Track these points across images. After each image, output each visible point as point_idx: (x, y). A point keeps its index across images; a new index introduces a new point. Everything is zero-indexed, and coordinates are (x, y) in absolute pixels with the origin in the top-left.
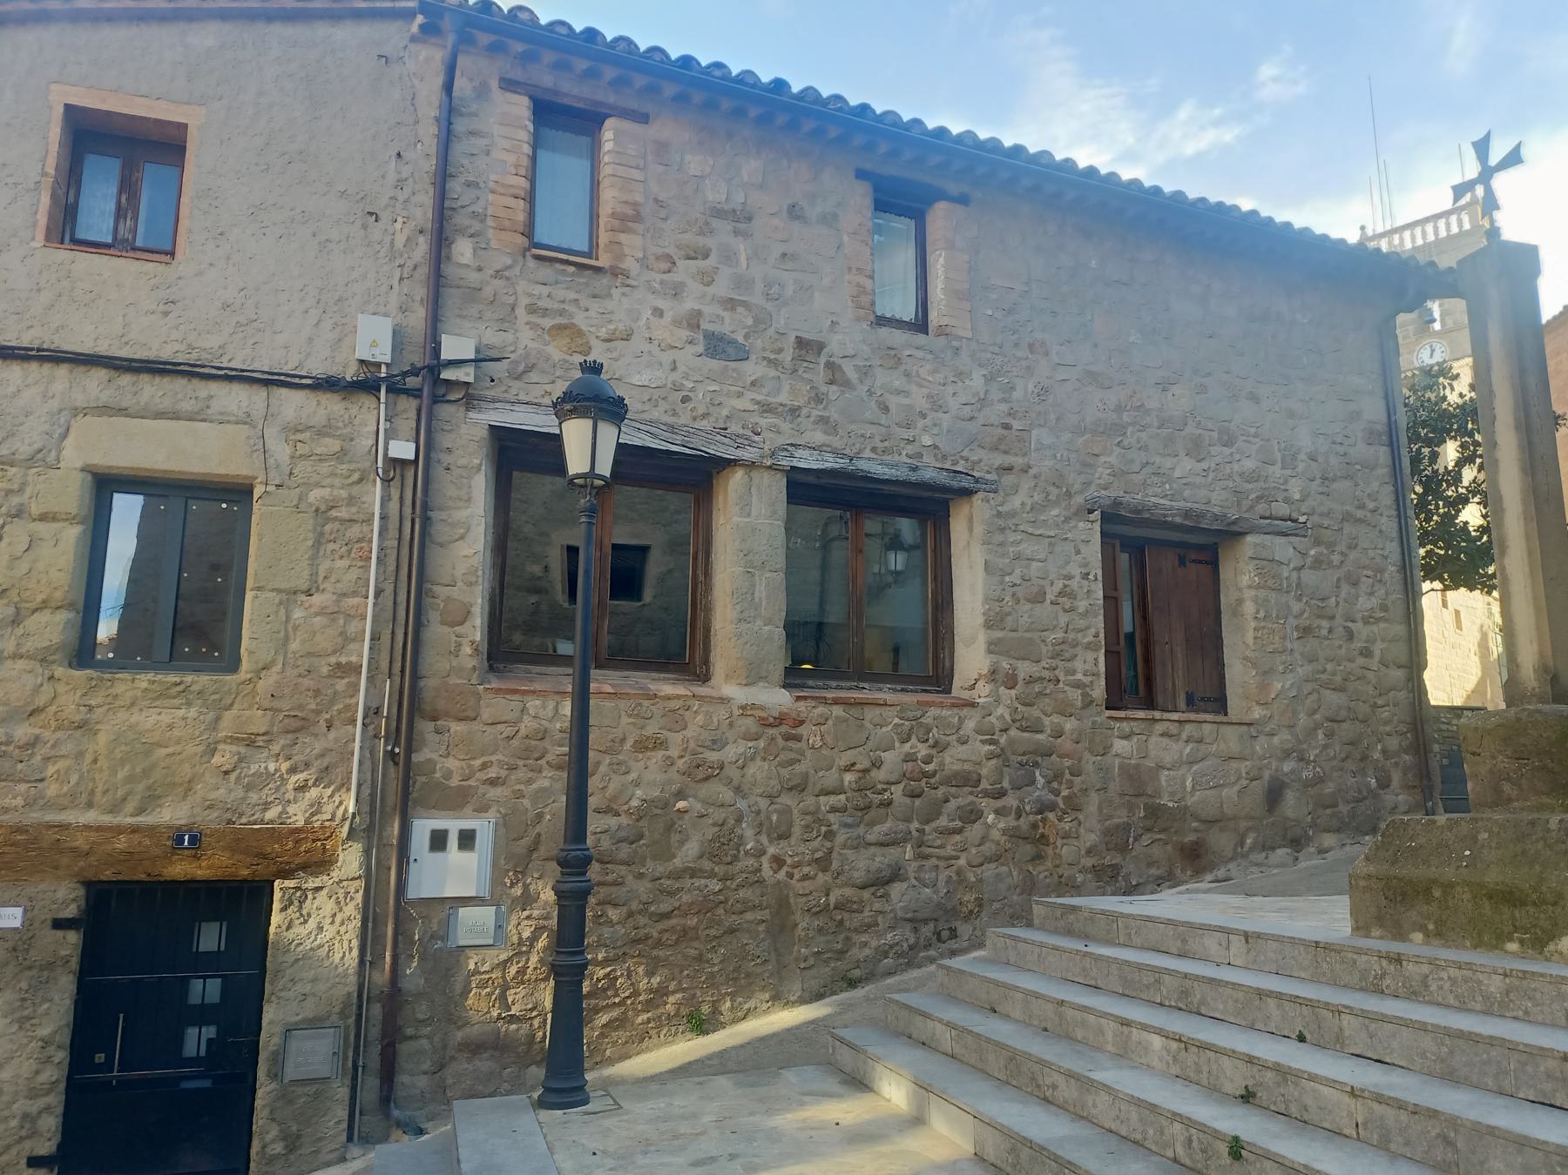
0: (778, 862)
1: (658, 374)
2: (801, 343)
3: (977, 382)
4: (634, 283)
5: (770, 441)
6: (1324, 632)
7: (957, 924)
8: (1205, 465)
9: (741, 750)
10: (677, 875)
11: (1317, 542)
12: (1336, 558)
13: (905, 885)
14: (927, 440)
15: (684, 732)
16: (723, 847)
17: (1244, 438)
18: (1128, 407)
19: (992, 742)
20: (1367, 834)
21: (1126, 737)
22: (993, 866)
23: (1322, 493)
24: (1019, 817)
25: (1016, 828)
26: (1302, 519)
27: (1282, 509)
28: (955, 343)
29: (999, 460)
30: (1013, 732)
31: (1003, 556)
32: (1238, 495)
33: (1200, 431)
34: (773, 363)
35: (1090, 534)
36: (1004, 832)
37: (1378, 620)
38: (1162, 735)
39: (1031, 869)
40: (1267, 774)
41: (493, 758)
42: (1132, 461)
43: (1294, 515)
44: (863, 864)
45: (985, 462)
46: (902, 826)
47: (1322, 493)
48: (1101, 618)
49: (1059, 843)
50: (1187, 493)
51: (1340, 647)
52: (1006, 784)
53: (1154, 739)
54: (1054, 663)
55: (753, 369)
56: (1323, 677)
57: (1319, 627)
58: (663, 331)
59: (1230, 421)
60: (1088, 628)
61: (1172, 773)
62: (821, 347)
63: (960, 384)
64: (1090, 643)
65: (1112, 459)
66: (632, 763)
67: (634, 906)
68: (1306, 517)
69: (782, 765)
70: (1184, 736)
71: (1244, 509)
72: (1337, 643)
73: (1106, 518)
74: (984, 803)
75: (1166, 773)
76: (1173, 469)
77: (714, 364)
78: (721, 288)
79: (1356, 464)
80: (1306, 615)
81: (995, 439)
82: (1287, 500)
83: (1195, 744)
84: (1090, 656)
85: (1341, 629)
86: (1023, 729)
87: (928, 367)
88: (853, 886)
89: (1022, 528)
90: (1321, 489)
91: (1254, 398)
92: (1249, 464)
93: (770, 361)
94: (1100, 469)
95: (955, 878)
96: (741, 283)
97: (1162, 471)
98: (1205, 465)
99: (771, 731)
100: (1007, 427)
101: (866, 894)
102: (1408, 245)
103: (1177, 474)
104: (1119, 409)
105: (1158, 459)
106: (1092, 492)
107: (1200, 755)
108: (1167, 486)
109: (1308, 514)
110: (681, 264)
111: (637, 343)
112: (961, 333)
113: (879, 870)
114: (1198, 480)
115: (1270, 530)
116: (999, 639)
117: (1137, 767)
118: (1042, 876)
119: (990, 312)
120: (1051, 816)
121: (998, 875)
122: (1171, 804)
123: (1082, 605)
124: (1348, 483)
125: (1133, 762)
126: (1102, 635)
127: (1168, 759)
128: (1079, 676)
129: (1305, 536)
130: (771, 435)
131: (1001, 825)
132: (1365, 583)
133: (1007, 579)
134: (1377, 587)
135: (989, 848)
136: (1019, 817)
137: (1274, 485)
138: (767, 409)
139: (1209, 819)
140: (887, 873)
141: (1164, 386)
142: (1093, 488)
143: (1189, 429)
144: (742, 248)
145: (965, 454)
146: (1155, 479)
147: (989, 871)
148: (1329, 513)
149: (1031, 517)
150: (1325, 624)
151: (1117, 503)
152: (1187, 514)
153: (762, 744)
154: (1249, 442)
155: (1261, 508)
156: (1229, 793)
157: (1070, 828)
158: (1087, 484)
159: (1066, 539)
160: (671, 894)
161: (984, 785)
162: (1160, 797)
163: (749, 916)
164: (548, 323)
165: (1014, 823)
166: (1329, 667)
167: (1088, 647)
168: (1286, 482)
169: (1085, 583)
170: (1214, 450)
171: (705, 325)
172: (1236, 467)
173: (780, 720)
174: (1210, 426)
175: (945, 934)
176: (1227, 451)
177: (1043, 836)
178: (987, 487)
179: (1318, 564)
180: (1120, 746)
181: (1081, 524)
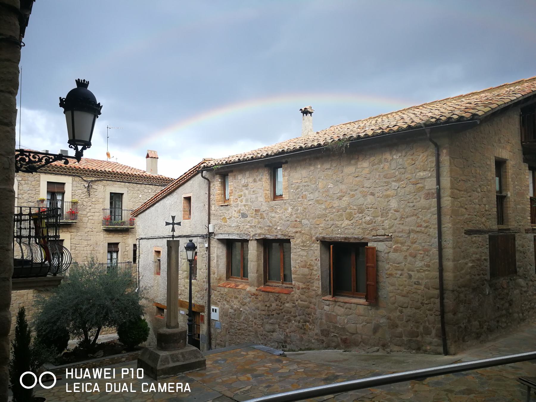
8: (352, 222)
21: (328, 305)
30: (299, 301)
104: (325, 209)
141: (340, 198)
143: (348, 211)
152: (345, 238)
174: (355, 208)
176: (361, 215)
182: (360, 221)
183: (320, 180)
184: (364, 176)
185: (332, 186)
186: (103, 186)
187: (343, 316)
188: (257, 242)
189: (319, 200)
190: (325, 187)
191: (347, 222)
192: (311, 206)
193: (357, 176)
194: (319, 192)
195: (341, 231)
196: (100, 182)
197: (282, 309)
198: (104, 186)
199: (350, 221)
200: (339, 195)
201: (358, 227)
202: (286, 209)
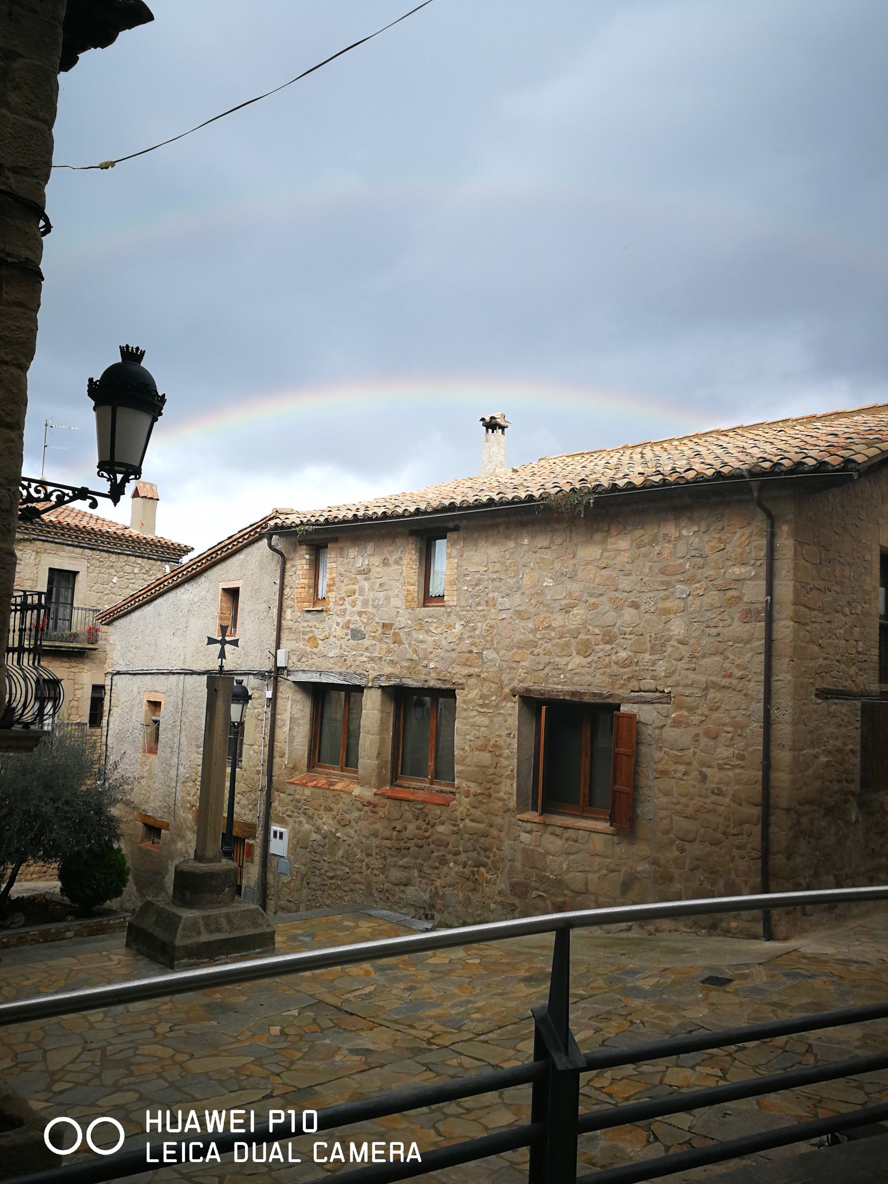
0: (368, 867)
1: (337, 651)
2: (384, 625)
3: (458, 628)
4: (332, 613)
5: (372, 674)
6: (679, 775)
7: (435, 913)
8: (589, 659)
9: (357, 815)
10: (335, 863)
11: (679, 706)
12: (695, 719)
13: (413, 888)
14: (432, 665)
15: (753, 826)
16: (347, 856)
17: (622, 636)
18: (540, 629)
19: (454, 825)
20: (704, 928)
21: (530, 832)
22: (451, 889)
23: (687, 669)
24: (464, 867)
25: (463, 872)
26: (666, 691)
27: (649, 684)
28: (449, 610)
29: (466, 671)
30: (467, 821)
31: (466, 724)
32: (614, 677)
33: (588, 637)
34: (374, 638)
35: (512, 707)
36: (457, 873)
37: (734, 767)
38: (551, 834)
39: (470, 895)
40: (624, 869)
41: (289, 807)
42: (539, 663)
43: (660, 688)
44: (396, 874)
45: (458, 672)
46: (412, 861)
47: (687, 669)
48: (516, 760)
49: (484, 884)
50: (576, 679)
51: (694, 786)
52: (461, 849)
53: (546, 836)
54: (488, 785)
55: (367, 642)
56: (678, 807)
57: (676, 771)
58: (340, 632)
59: (614, 626)
60: (509, 766)
61: (554, 858)
62: (391, 625)
63: (449, 632)
64: (509, 775)
65: (526, 664)
66: (324, 815)
67: (323, 871)
68: (670, 689)
69: (370, 824)
70: (566, 835)
71: (617, 687)
72: (692, 782)
73: (521, 697)
74: (450, 856)
75: (551, 857)
76: (567, 664)
77: (353, 642)
78: (358, 608)
79: (729, 641)
80: (664, 761)
81: (464, 660)
82: (653, 678)
83: (572, 842)
84: (509, 782)
85: (696, 773)
86: (472, 820)
87: (434, 625)
88: (391, 883)
89: (476, 708)
90: (687, 666)
91: (635, 605)
92: (623, 654)
93: (373, 637)
94: (520, 670)
95: (434, 890)
96: (365, 603)
97: (560, 667)
98: (589, 659)
99: (366, 808)
100: (470, 652)
101: (397, 888)
102: (789, 677)
103: (570, 667)
104: (535, 631)
105: (557, 659)
106: (515, 684)
107: (575, 849)
108: (562, 676)
109: (672, 686)
110: (347, 599)
111: (332, 639)
112: (451, 604)
113: (401, 879)
114: (583, 671)
115: (639, 699)
116: (462, 770)
117: (533, 850)
118: (475, 900)
119: (466, 588)
120: (482, 869)
121: (452, 894)
122: (551, 877)
123: (506, 752)
124: (717, 658)
125: (531, 847)
126: (515, 771)
127: (553, 849)
128: (502, 794)
129: (669, 704)
130: (372, 672)
131: (456, 869)
132: (724, 737)
133: (467, 737)
134: (738, 739)
135: (449, 880)
136: (464, 867)
137: (643, 667)
138: (372, 659)
139: (576, 890)
140: (405, 881)
141: (566, 609)
142: (516, 681)
143: (582, 636)
144: (366, 585)
145: (450, 670)
146: (554, 672)
147: (449, 891)
148: (692, 684)
149: (481, 702)
150: (682, 768)
151: (527, 690)
152: (574, 694)
153: (362, 813)
154: (626, 639)
155: (634, 684)
156: (593, 877)
157: (491, 878)
158: (512, 680)
159: (499, 713)
160: (334, 870)
161: (450, 847)
162: (545, 871)
163: (358, 886)
164: (307, 637)
165: (461, 870)
166: (683, 800)
167: (508, 777)
168: (654, 665)
169: (508, 739)
170: (597, 648)
171: (352, 626)
172: (614, 657)
173: (369, 803)
174: (597, 631)
175: (429, 916)
176: (608, 647)
177: (476, 879)
178: (459, 687)
179: (677, 723)
180: (525, 837)
181: (509, 704)
182: (607, 659)
183: (527, 570)
184: (619, 567)
185: (551, 585)
186: (34, 553)
187: (560, 856)
188: (382, 691)
189: (522, 611)
190: (535, 586)
191: (578, 660)
192: (505, 622)
193: (604, 565)
194: (523, 594)
195: (565, 677)
196: (28, 543)
197: (428, 838)
198: (37, 553)
199: (586, 657)
200: (564, 602)
201: (602, 670)
202: (450, 627)
